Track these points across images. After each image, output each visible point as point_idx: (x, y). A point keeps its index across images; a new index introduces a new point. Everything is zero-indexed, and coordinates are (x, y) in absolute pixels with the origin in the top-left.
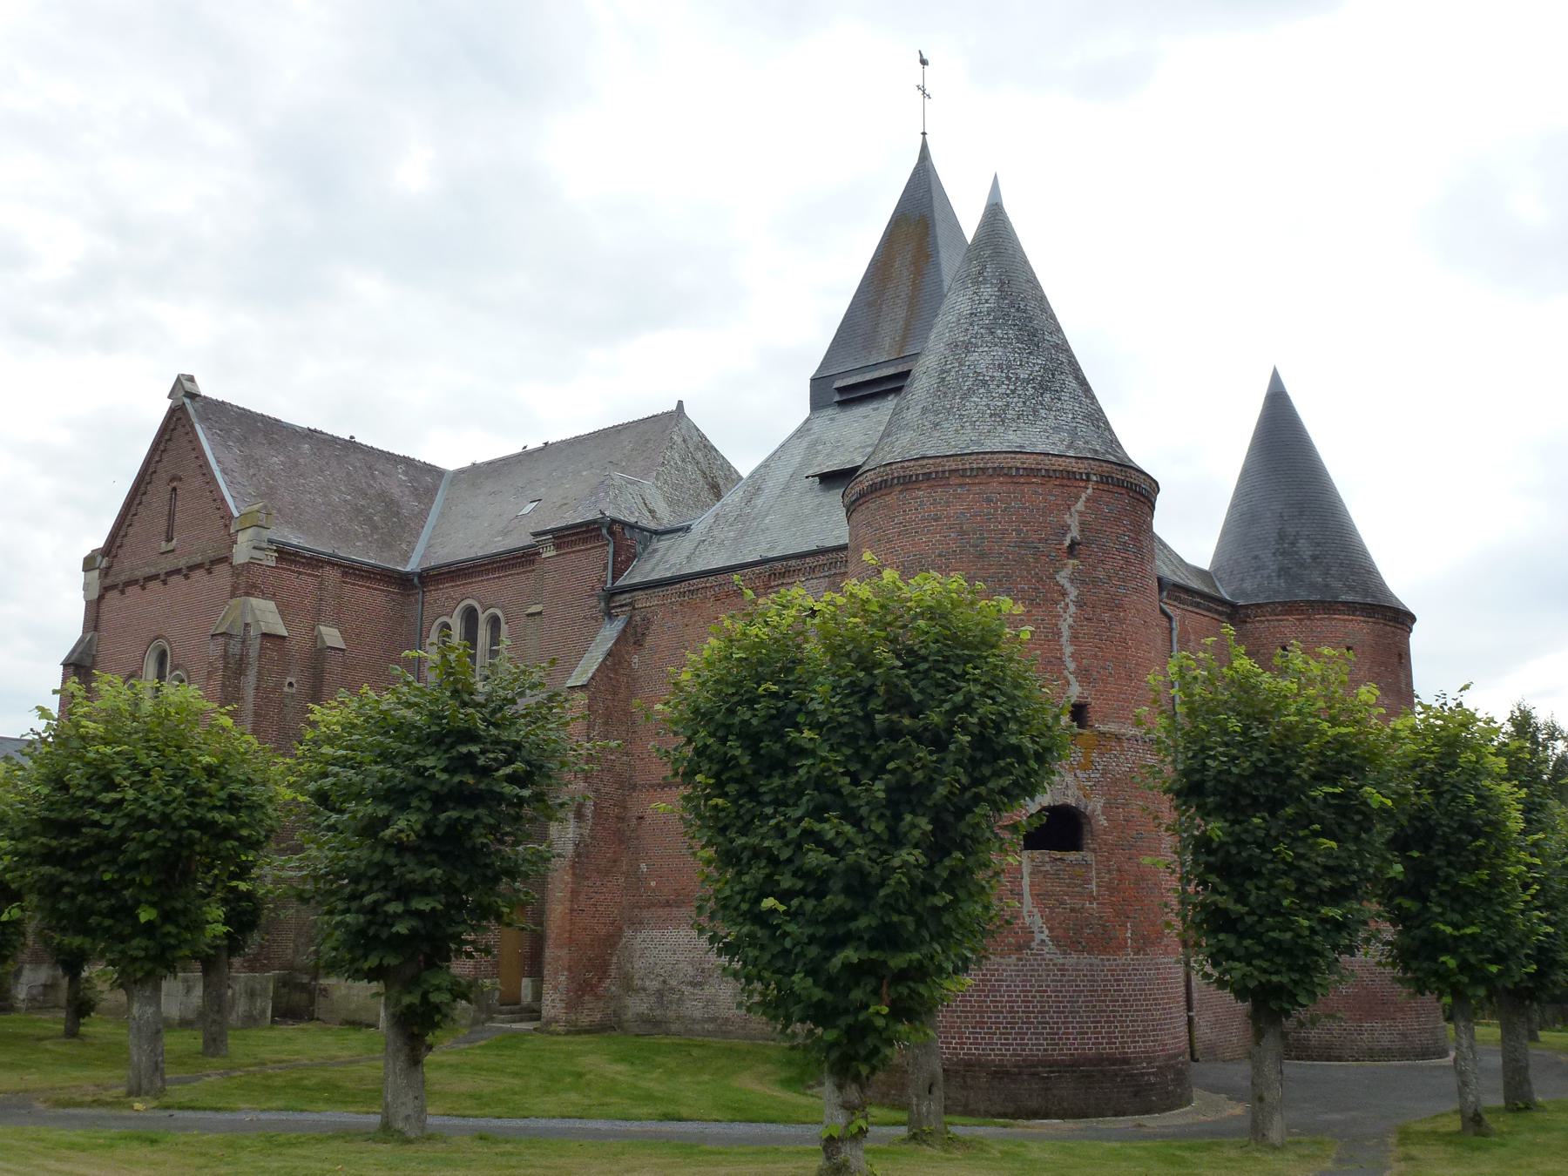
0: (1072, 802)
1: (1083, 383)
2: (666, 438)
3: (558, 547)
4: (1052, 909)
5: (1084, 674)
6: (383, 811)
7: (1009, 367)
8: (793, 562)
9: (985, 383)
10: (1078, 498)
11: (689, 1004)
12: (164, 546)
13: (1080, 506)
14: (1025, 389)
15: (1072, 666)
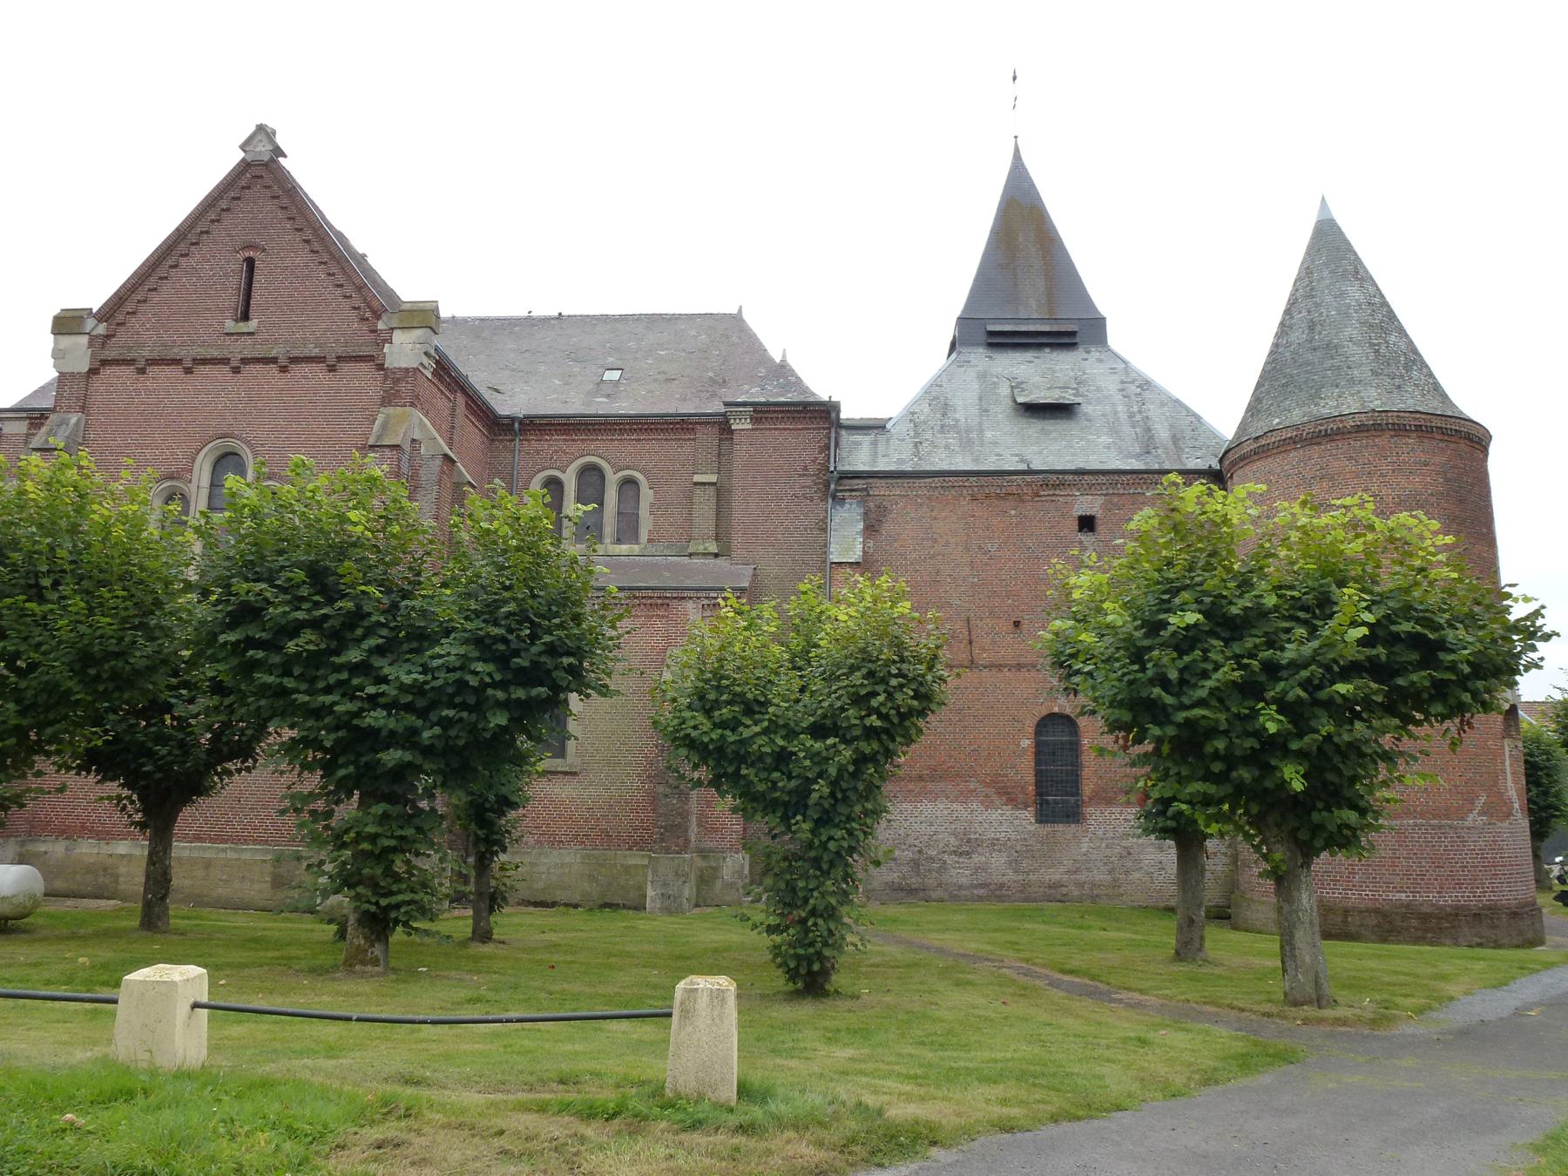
3: (755, 420)
6: (377, 662)
11: (954, 872)
12: (230, 325)
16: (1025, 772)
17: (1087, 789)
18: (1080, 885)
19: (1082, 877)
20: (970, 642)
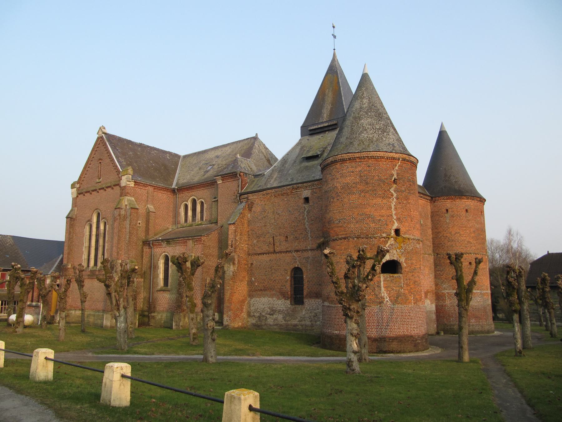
0: (395, 259)
1: (395, 129)
2: (250, 146)
3: (223, 180)
4: (390, 291)
5: (398, 220)
7: (373, 125)
8: (300, 185)
9: (366, 130)
10: (396, 166)
11: (269, 320)
13: (397, 168)
14: (378, 132)
15: (395, 217)
16: (288, 288)
17: (305, 293)
18: (302, 326)
19: (303, 323)
20: (274, 245)
